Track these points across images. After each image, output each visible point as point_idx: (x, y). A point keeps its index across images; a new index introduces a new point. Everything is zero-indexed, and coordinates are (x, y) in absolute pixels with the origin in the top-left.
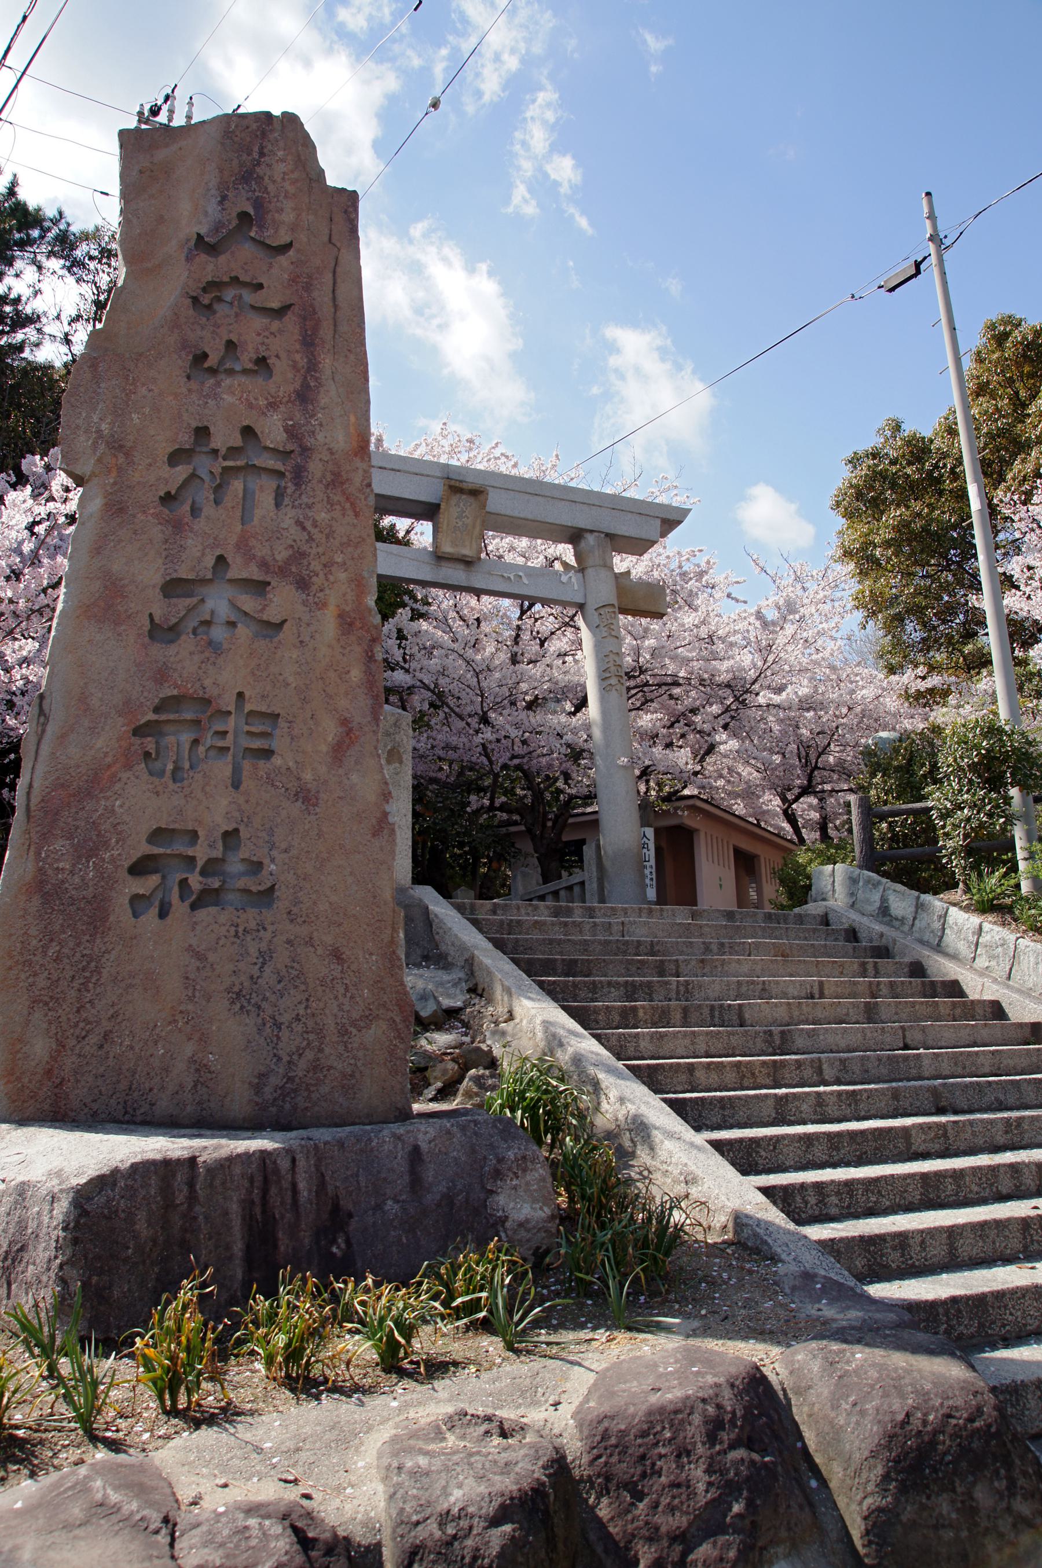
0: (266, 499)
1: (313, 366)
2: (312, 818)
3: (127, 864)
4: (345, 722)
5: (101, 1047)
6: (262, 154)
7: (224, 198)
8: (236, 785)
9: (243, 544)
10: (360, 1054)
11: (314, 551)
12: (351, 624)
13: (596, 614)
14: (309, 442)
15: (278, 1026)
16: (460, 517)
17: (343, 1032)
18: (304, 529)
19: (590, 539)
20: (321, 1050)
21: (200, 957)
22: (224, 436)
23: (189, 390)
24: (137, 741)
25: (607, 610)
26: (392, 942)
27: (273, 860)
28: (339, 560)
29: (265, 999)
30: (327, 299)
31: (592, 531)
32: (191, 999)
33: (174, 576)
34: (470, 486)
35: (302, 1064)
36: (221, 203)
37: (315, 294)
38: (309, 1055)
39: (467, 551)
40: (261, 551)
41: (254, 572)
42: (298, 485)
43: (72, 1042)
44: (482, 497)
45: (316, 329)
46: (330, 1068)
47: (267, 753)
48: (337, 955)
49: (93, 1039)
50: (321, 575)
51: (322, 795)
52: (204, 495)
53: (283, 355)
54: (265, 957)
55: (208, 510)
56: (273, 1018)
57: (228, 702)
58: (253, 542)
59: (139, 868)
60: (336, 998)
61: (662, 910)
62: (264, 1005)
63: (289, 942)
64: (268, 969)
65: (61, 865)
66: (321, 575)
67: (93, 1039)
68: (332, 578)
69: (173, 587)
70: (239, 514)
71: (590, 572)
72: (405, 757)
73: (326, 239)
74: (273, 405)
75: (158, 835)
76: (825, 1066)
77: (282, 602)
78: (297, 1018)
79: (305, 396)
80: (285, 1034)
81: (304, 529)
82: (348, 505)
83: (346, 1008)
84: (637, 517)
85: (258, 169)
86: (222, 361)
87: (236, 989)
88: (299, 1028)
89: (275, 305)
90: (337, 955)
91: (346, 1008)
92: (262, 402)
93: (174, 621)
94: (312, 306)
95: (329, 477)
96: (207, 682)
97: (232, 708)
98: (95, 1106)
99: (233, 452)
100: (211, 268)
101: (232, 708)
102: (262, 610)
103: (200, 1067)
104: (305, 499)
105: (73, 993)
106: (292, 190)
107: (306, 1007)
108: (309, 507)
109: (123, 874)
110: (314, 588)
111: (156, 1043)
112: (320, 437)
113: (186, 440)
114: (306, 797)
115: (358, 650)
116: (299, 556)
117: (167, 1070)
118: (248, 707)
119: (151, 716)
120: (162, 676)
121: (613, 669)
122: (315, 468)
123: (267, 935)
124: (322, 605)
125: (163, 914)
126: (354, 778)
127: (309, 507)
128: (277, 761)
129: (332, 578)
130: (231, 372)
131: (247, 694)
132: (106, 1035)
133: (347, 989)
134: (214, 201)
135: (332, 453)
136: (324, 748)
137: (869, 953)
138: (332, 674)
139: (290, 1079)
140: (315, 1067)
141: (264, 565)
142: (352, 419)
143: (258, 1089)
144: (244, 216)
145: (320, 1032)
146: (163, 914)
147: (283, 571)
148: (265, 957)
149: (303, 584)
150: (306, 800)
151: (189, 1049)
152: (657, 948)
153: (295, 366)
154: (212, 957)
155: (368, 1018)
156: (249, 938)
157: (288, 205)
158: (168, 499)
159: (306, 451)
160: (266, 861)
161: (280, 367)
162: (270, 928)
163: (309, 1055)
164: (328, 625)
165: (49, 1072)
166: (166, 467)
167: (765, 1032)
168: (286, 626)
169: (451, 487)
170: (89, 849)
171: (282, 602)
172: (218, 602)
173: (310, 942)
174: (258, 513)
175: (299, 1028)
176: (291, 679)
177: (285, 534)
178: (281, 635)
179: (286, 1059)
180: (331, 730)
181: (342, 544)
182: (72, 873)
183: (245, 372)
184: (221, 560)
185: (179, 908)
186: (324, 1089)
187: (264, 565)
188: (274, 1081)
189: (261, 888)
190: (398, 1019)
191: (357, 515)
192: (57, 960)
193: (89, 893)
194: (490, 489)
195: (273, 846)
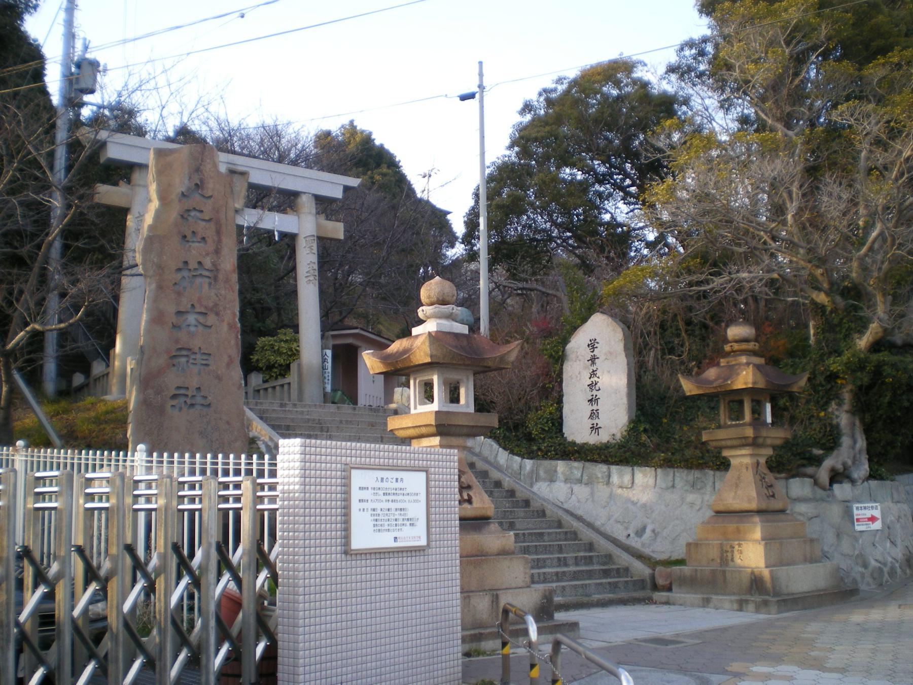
1: (220, 241)
4: (230, 356)
14: (219, 267)
48: (228, 423)
57: (196, 350)
89: (207, 218)
90: (228, 423)
113: (181, 265)
120: (177, 341)
122: (221, 276)
141: (206, 307)
147: (211, 310)
149: (217, 314)
161: (209, 240)
164: (225, 328)
172: (191, 318)
173: (221, 419)
180: (226, 359)
187: (206, 307)
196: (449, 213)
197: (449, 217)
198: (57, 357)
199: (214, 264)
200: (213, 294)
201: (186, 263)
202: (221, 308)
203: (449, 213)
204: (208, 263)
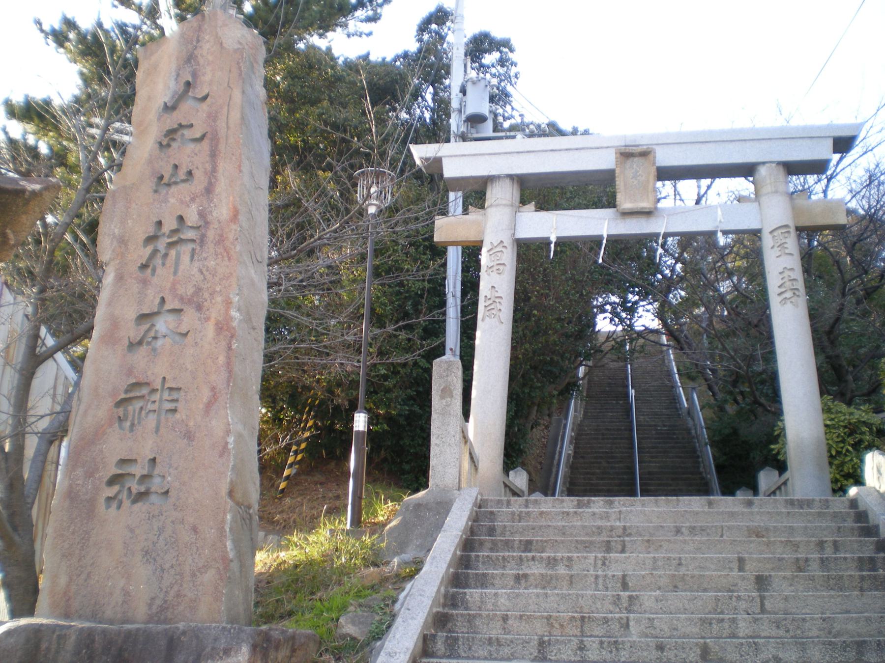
0: (186, 259)
1: (214, 170)
2: (191, 448)
3: (105, 480)
4: (213, 389)
5: (86, 580)
6: (198, 41)
7: (178, 75)
8: (157, 430)
9: (173, 289)
10: (200, 588)
11: (205, 287)
12: (221, 329)
13: (770, 236)
14: (209, 218)
15: (163, 570)
16: (635, 177)
17: (194, 575)
18: (202, 273)
19: (763, 171)
20: (181, 586)
21: (132, 531)
22: (170, 224)
23: (154, 200)
24: (115, 410)
25: (780, 231)
26: (223, 521)
27: (170, 474)
28: (218, 289)
29: (158, 555)
30: (224, 125)
31: (764, 163)
32: (125, 555)
33: (141, 312)
34: (639, 149)
35: (172, 593)
36: (176, 79)
37: (218, 122)
38: (176, 588)
39: (645, 205)
40: (181, 291)
41: (176, 305)
42: (201, 246)
43: (75, 578)
44: (651, 157)
45: (217, 145)
46: (185, 596)
47: (174, 411)
48: (195, 529)
49: (83, 576)
50: (209, 301)
51: (197, 435)
52: (158, 261)
53: (200, 166)
54: (161, 530)
55: (159, 271)
56: (161, 566)
57: (158, 385)
58: (178, 286)
59: (114, 480)
60: (192, 555)
61: (678, 500)
62: (158, 559)
63: (173, 522)
64: (161, 538)
65: (78, 482)
66: (209, 301)
67: (83, 576)
68: (213, 301)
69: (143, 317)
70: (172, 270)
71: (764, 200)
72: (454, 392)
73: (226, 85)
74: (193, 200)
75: (123, 462)
76: (632, 623)
77: (190, 318)
78: (172, 567)
79: (209, 190)
80: (166, 575)
81: (202, 273)
82: (225, 254)
83: (196, 561)
84: (809, 142)
85: (195, 52)
86: (170, 179)
87: (145, 549)
88: (172, 572)
89: (198, 136)
90: (195, 529)
91: (196, 561)
92: (188, 199)
93: (138, 339)
94: (216, 131)
95: (217, 238)
96: (149, 373)
97: (159, 387)
98: (81, 612)
99: (175, 232)
100: (171, 120)
101: (159, 387)
102: (177, 327)
103: (126, 593)
104: (204, 255)
105: (77, 552)
106: (210, 58)
107: (177, 560)
108: (205, 259)
109: (104, 486)
110: (205, 308)
111: (108, 579)
112: (214, 214)
113: (151, 231)
114: (189, 436)
115: (224, 343)
116: (198, 290)
117: (111, 594)
118: (167, 386)
119: (123, 396)
120: (130, 372)
121: (788, 284)
122: (211, 234)
123: (162, 518)
124: (207, 319)
125: (119, 507)
126: (214, 422)
127: (205, 259)
128: (178, 416)
129: (213, 301)
130: (176, 183)
131: (167, 377)
132: (89, 575)
133: (197, 550)
134: (173, 79)
135: (220, 223)
136: (201, 406)
137: (856, 533)
138: (209, 361)
139: (166, 602)
140: (178, 595)
141: (182, 299)
142: (231, 198)
143: (150, 606)
144: (188, 84)
145: (181, 574)
146: (119, 507)
147: (190, 301)
148: (161, 530)
149: (199, 308)
150: (189, 437)
151: (122, 583)
152: (629, 531)
153: (206, 173)
154: (137, 531)
155: (206, 567)
156: (154, 520)
157: (208, 69)
158: (144, 267)
159: (207, 223)
160: (167, 475)
161: (198, 174)
162: (165, 514)
163: (176, 588)
164: (210, 330)
165: (65, 593)
166: (142, 249)
167: (613, 596)
168: (190, 334)
169: (622, 154)
170: (90, 474)
171: (190, 318)
172: (162, 325)
173: (182, 522)
174: (182, 267)
175: (172, 572)
176: (189, 366)
177: (193, 278)
178: (186, 340)
179: (165, 590)
180: (206, 394)
181: (220, 279)
182: (83, 486)
183: (183, 181)
184: (163, 300)
185: (127, 503)
186: (181, 608)
187: (182, 299)
188: (158, 602)
189: (163, 491)
190: (221, 568)
191: (229, 259)
192: (73, 533)
193: (87, 497)
194: (657, 148)
195: (171, 466)
196: (368, 54)
197: (372, 58)
198: (311, 563)
199: (202, 215)
200: (195, 271)
201: (181, 219)
202: (206, 295)
203: (368, 54)
204: (192, 218)
